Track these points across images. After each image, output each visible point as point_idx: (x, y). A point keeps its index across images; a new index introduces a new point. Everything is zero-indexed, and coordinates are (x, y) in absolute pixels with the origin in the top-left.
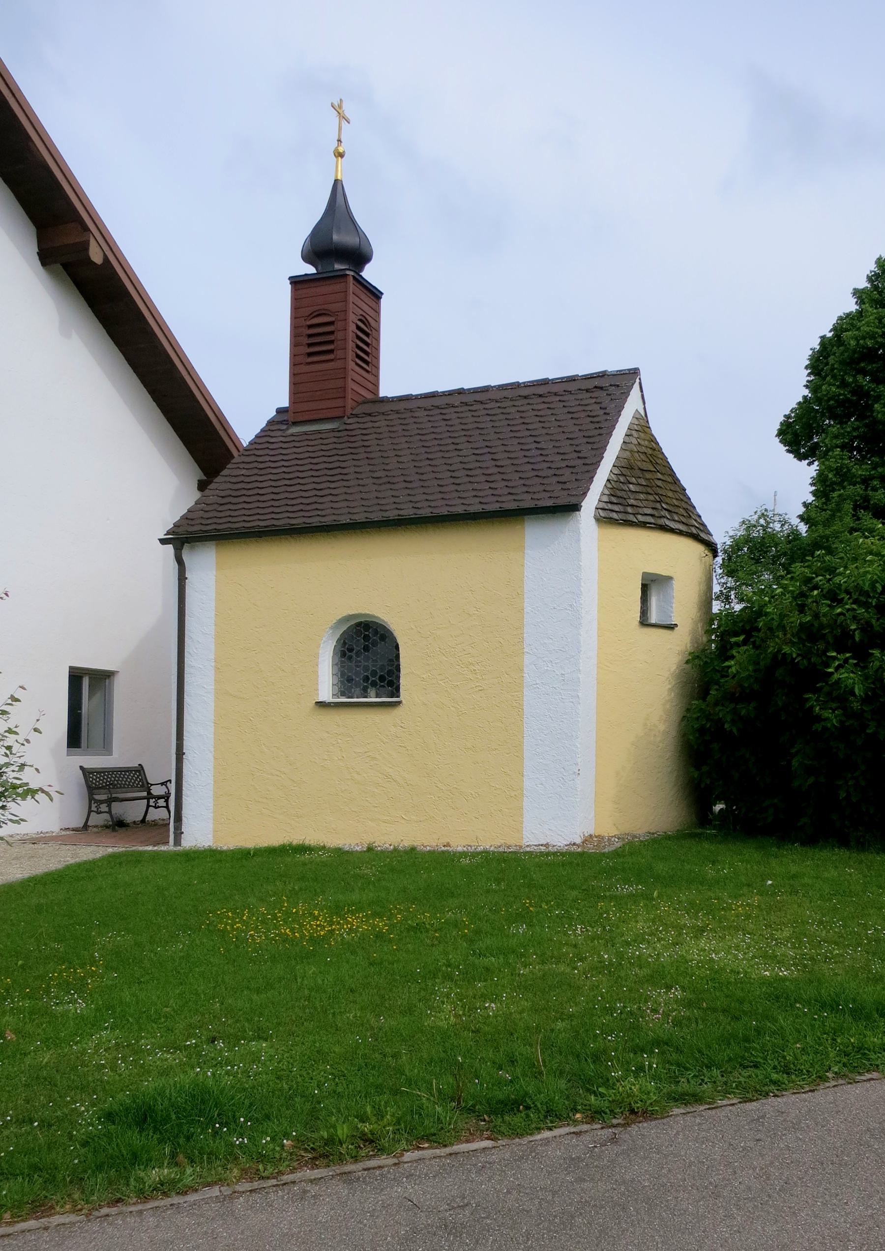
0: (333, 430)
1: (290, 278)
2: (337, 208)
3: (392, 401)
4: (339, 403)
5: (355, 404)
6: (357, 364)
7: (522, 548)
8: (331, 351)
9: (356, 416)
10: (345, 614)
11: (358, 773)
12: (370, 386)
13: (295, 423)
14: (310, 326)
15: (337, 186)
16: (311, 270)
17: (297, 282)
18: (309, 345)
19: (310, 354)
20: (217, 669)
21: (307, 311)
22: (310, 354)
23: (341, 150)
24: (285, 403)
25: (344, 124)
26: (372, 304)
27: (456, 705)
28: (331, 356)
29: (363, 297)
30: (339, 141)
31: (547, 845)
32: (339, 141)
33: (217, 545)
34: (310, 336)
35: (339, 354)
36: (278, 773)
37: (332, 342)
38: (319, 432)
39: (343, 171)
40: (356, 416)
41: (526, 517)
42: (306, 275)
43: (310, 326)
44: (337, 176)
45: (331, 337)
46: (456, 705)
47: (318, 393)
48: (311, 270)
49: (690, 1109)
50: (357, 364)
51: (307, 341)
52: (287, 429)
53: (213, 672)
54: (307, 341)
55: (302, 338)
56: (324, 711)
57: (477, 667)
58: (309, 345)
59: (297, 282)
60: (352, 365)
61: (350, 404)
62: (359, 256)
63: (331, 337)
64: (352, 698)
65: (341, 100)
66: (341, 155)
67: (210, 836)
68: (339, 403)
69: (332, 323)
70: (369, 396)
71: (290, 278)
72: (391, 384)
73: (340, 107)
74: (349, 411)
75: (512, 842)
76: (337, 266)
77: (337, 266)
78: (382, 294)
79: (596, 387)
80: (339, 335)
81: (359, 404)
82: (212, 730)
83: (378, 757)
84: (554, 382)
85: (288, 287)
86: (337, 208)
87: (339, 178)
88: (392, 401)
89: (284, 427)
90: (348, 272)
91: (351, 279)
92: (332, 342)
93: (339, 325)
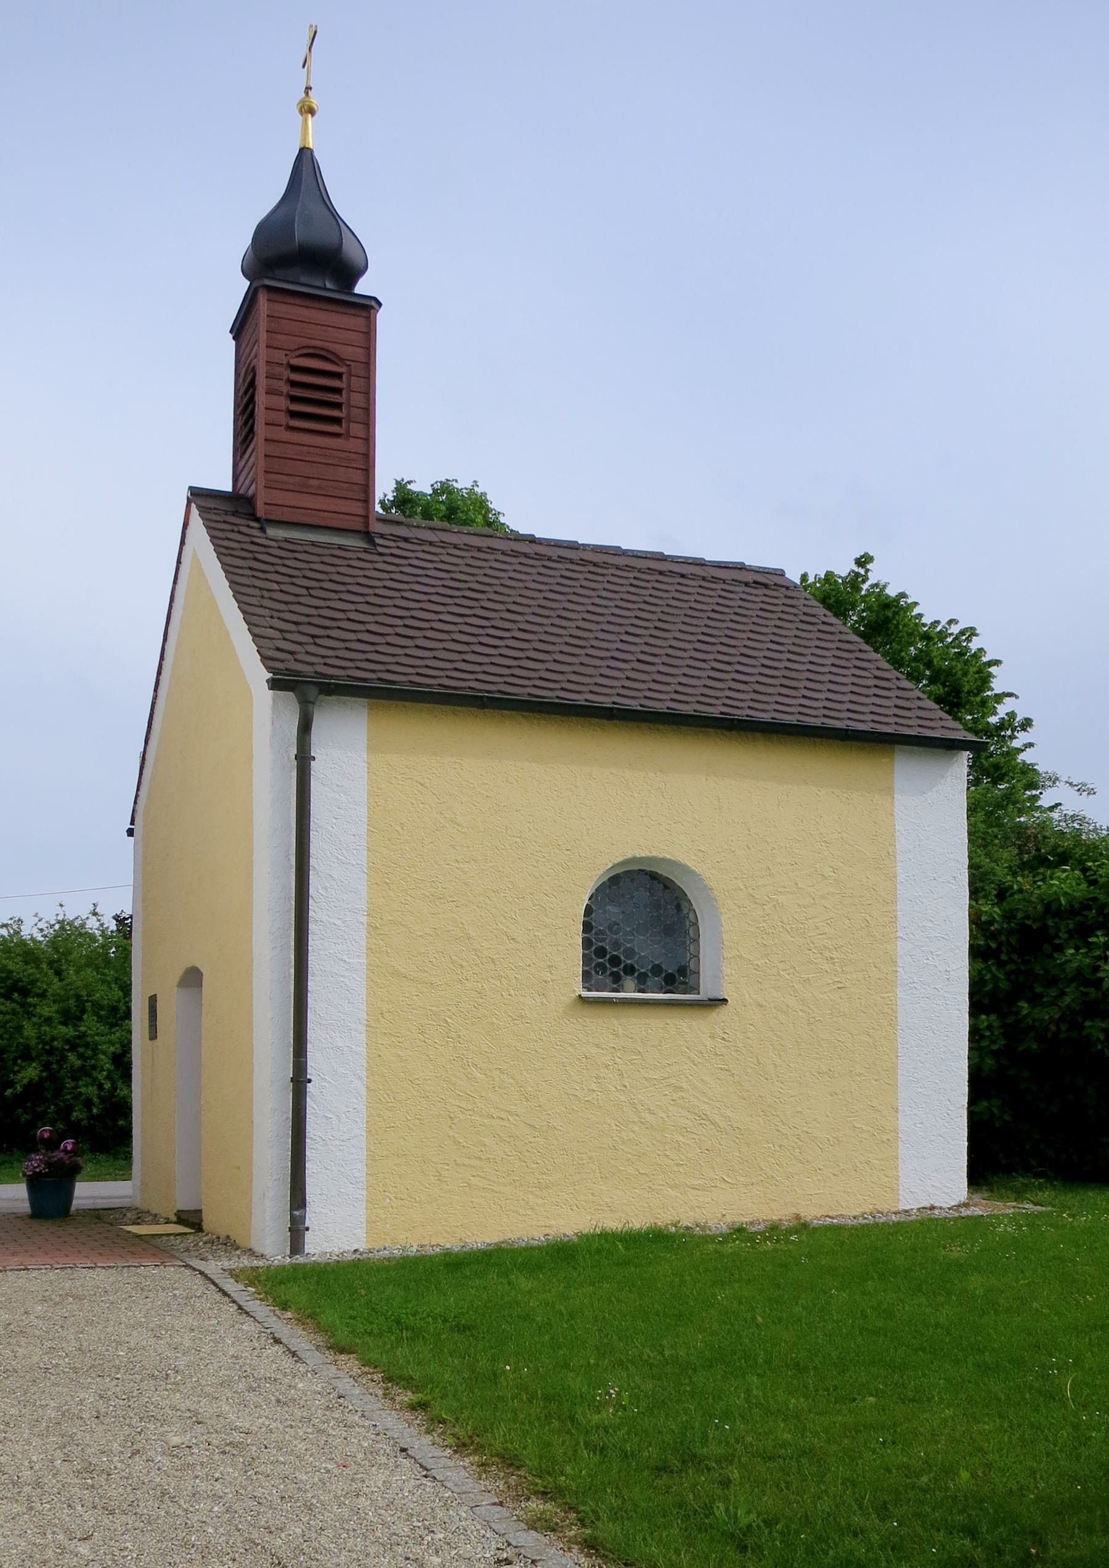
7: (889, 791)
8: (337, 421)
10: (629, 856)
11: (650, 1112)
15: (305, 166)
20: (372, 928)
22: (293, 414)
27: (805, 1009)
28: (335, 429)
31: (932, 1208)
33: (370, 707)
36: (504, 1115)
41: (897, 746)
46: (805, 1009)
49: (423, 1445)
51: (285, 388)
53: (364, 934)
56: (590, 1011)
57: (835, 954)
64: (643, 991)
67: (361, 1233)
75: (885, 1207)
79: (755, 582)
82: (363, 1037)
83: (684, 1085)
84: (625, 553)
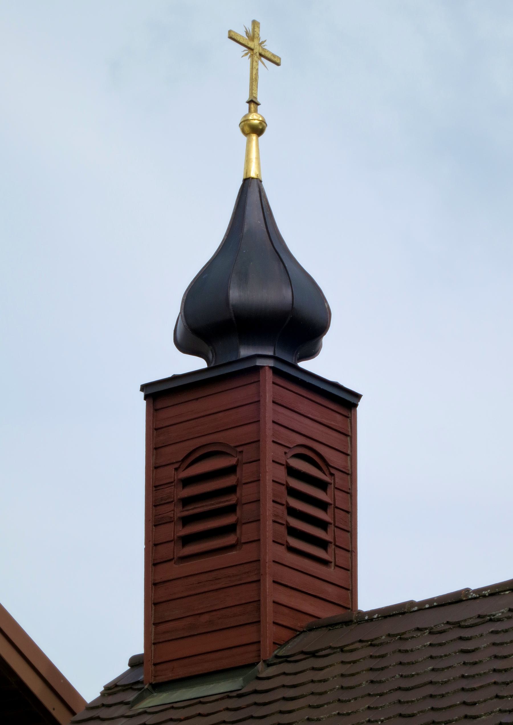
0: (227, 696)
1: (144, 388)
2: (251, 229)
3: (371, 620)
4: (248, 635)
5: (285, 634)
6: (291, 550)
8: (231, 529)
9: (286, 659)
12: (331, 592)
13: (158, 687)
14: (187, 482)
16: (198, 363)
17: (157, 394)
18: (186, 521)
19: (186, 540)
21: (180, 451)
22: (186, 540)
23: (255, 119)
24: (139, 649)
25: (265, 69)
26: (337, 420)
29: (305, 406)
30: (253, 102)
32: (253, 102)
34: (186, 502)
35: (246, 532)
37: (231, 509)
38: (199, 701)
39: (266, 161)
40: (286, 659)
42: (175, 378)
43: (187, 482)
44: (247, 170)
45: (231, 500)
47: (205, 618)
48: (198, 363)
50: (291, 550)
52: (139, 699)
54: (179, 512)
55: (171, 507)
58: (186, 521)
59: (157, 394)
60: (272, 552)
61: (270, 632)
62: (302, 325)
63: (231, 500)
65: (255, 23)
66: (258, 130)
68: (248, 635)
69: (231, 470)
70: (327, 613)
71: (144, 388)
72: (375, 591)
73: (252, 37)
74: (268, 651)
76: (245, 352)
77: (245, 352)
78: (358, 396)
80: (246, 493)
81: (297, 633)
85: (139, 405)
86: (251, 229)
87: (253, 174)
88: (371, 620)
89: (131, 696)
90: (259, 362)
91: (269, 376)
92: (231, 509)
93: (245, 472)
